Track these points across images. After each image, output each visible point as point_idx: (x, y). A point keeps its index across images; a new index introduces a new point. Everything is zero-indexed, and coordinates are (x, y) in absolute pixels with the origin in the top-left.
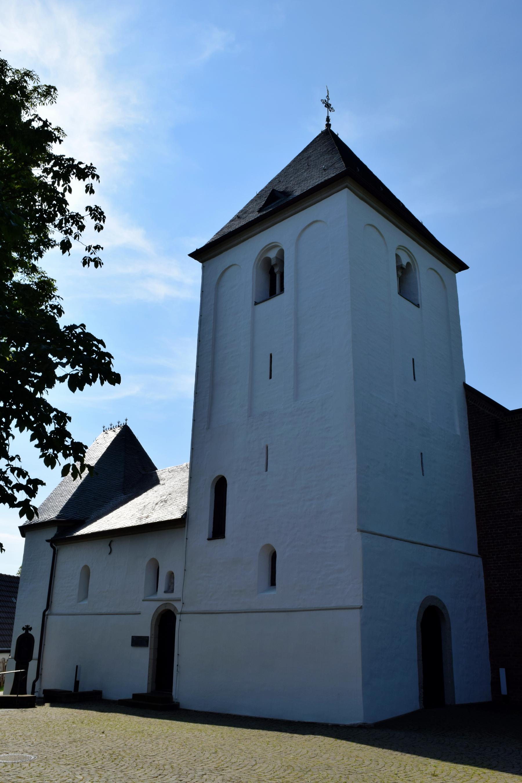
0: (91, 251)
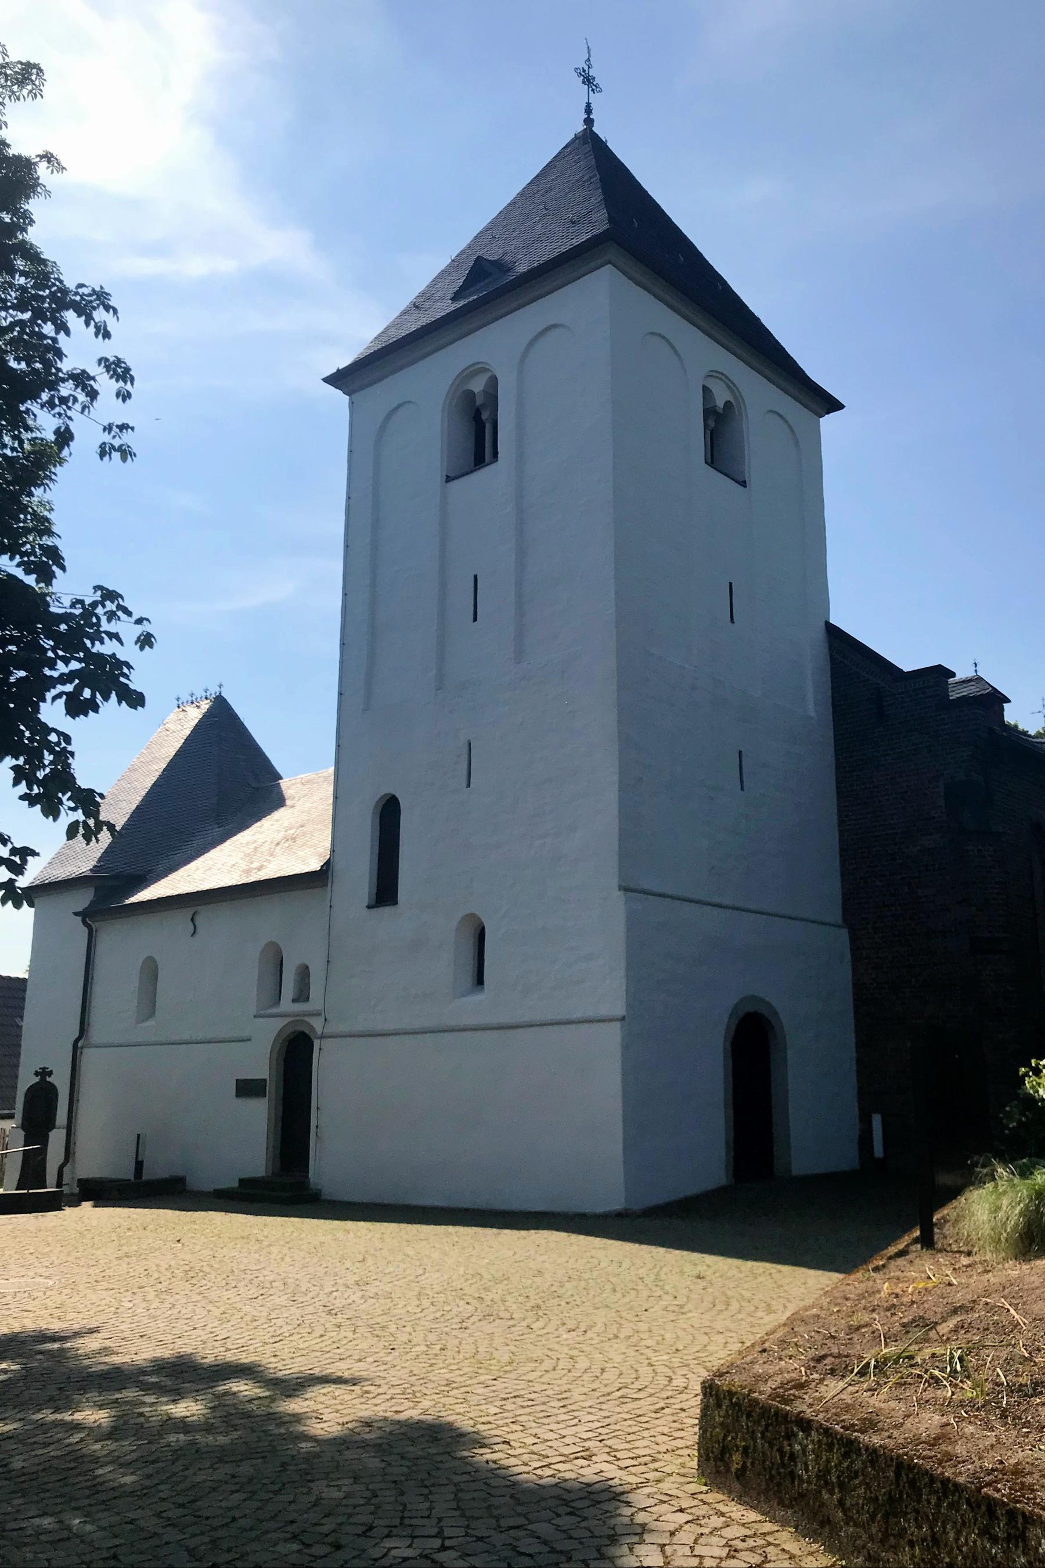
0: (113, 433)
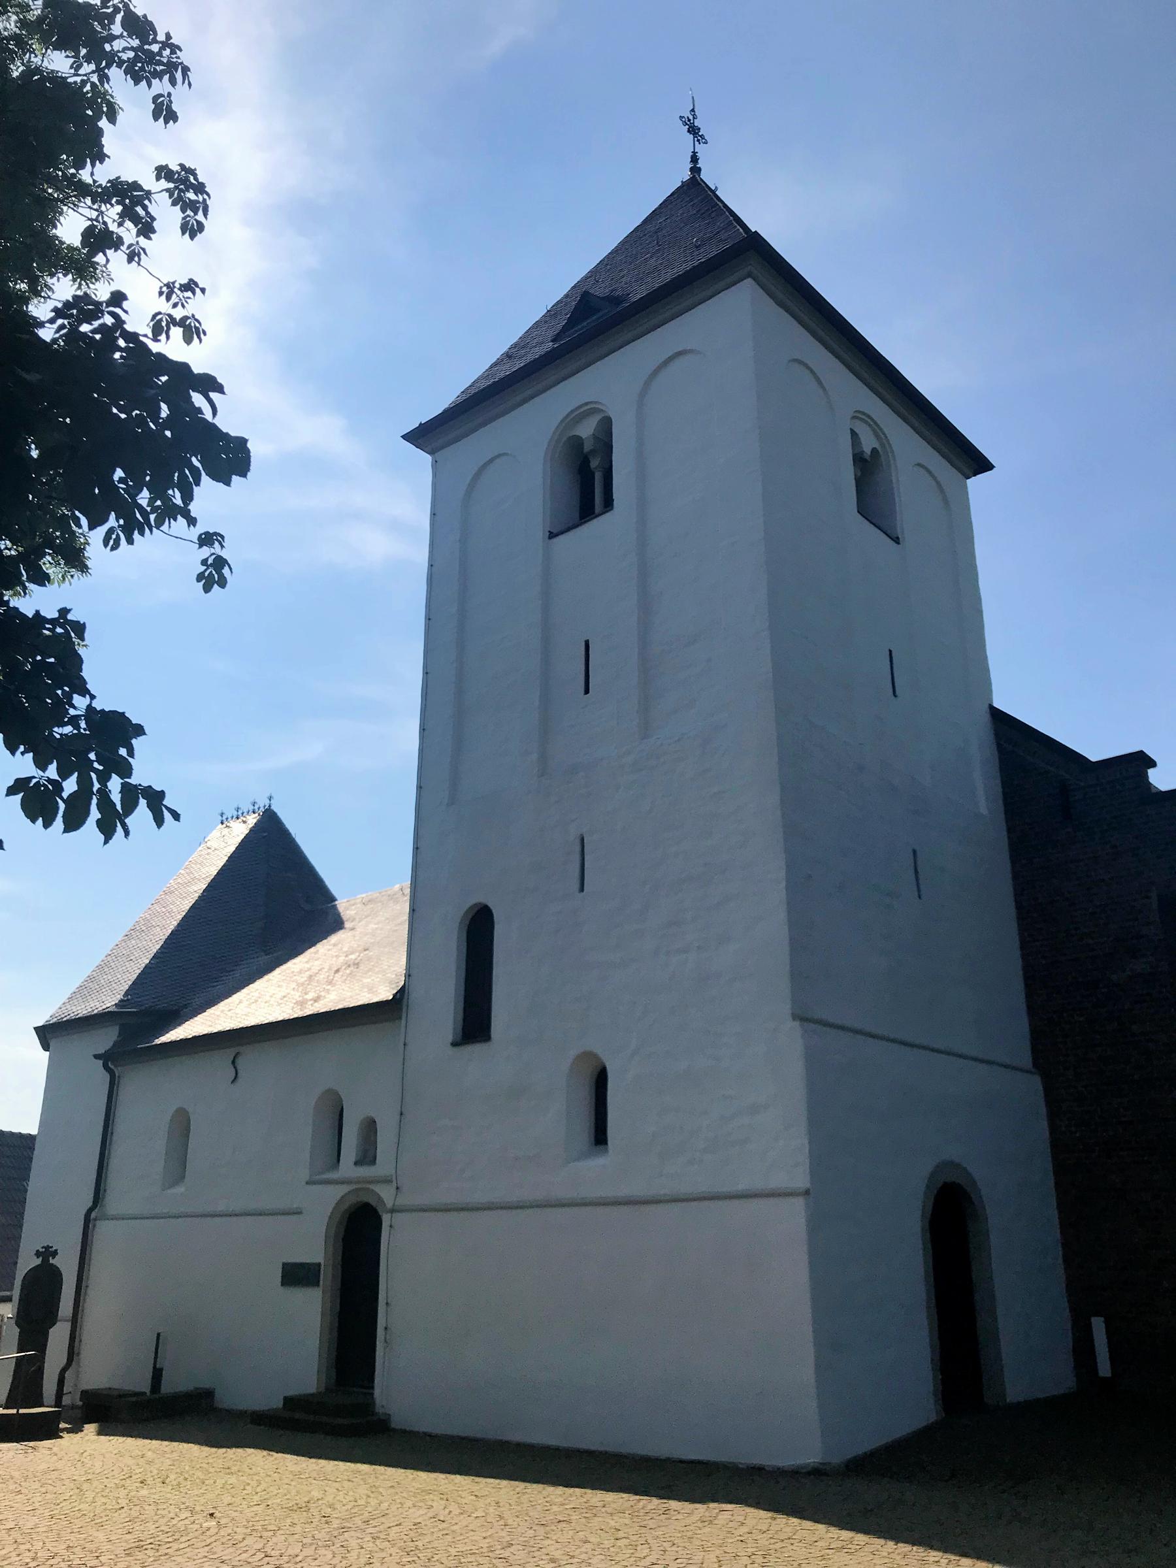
0: (174, 299)
